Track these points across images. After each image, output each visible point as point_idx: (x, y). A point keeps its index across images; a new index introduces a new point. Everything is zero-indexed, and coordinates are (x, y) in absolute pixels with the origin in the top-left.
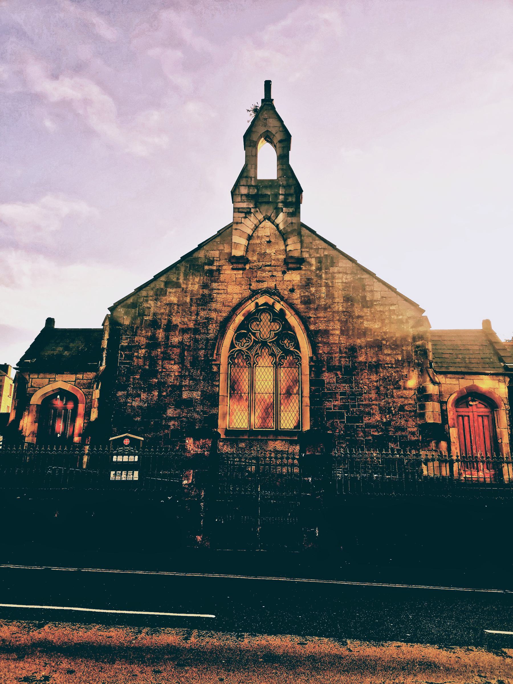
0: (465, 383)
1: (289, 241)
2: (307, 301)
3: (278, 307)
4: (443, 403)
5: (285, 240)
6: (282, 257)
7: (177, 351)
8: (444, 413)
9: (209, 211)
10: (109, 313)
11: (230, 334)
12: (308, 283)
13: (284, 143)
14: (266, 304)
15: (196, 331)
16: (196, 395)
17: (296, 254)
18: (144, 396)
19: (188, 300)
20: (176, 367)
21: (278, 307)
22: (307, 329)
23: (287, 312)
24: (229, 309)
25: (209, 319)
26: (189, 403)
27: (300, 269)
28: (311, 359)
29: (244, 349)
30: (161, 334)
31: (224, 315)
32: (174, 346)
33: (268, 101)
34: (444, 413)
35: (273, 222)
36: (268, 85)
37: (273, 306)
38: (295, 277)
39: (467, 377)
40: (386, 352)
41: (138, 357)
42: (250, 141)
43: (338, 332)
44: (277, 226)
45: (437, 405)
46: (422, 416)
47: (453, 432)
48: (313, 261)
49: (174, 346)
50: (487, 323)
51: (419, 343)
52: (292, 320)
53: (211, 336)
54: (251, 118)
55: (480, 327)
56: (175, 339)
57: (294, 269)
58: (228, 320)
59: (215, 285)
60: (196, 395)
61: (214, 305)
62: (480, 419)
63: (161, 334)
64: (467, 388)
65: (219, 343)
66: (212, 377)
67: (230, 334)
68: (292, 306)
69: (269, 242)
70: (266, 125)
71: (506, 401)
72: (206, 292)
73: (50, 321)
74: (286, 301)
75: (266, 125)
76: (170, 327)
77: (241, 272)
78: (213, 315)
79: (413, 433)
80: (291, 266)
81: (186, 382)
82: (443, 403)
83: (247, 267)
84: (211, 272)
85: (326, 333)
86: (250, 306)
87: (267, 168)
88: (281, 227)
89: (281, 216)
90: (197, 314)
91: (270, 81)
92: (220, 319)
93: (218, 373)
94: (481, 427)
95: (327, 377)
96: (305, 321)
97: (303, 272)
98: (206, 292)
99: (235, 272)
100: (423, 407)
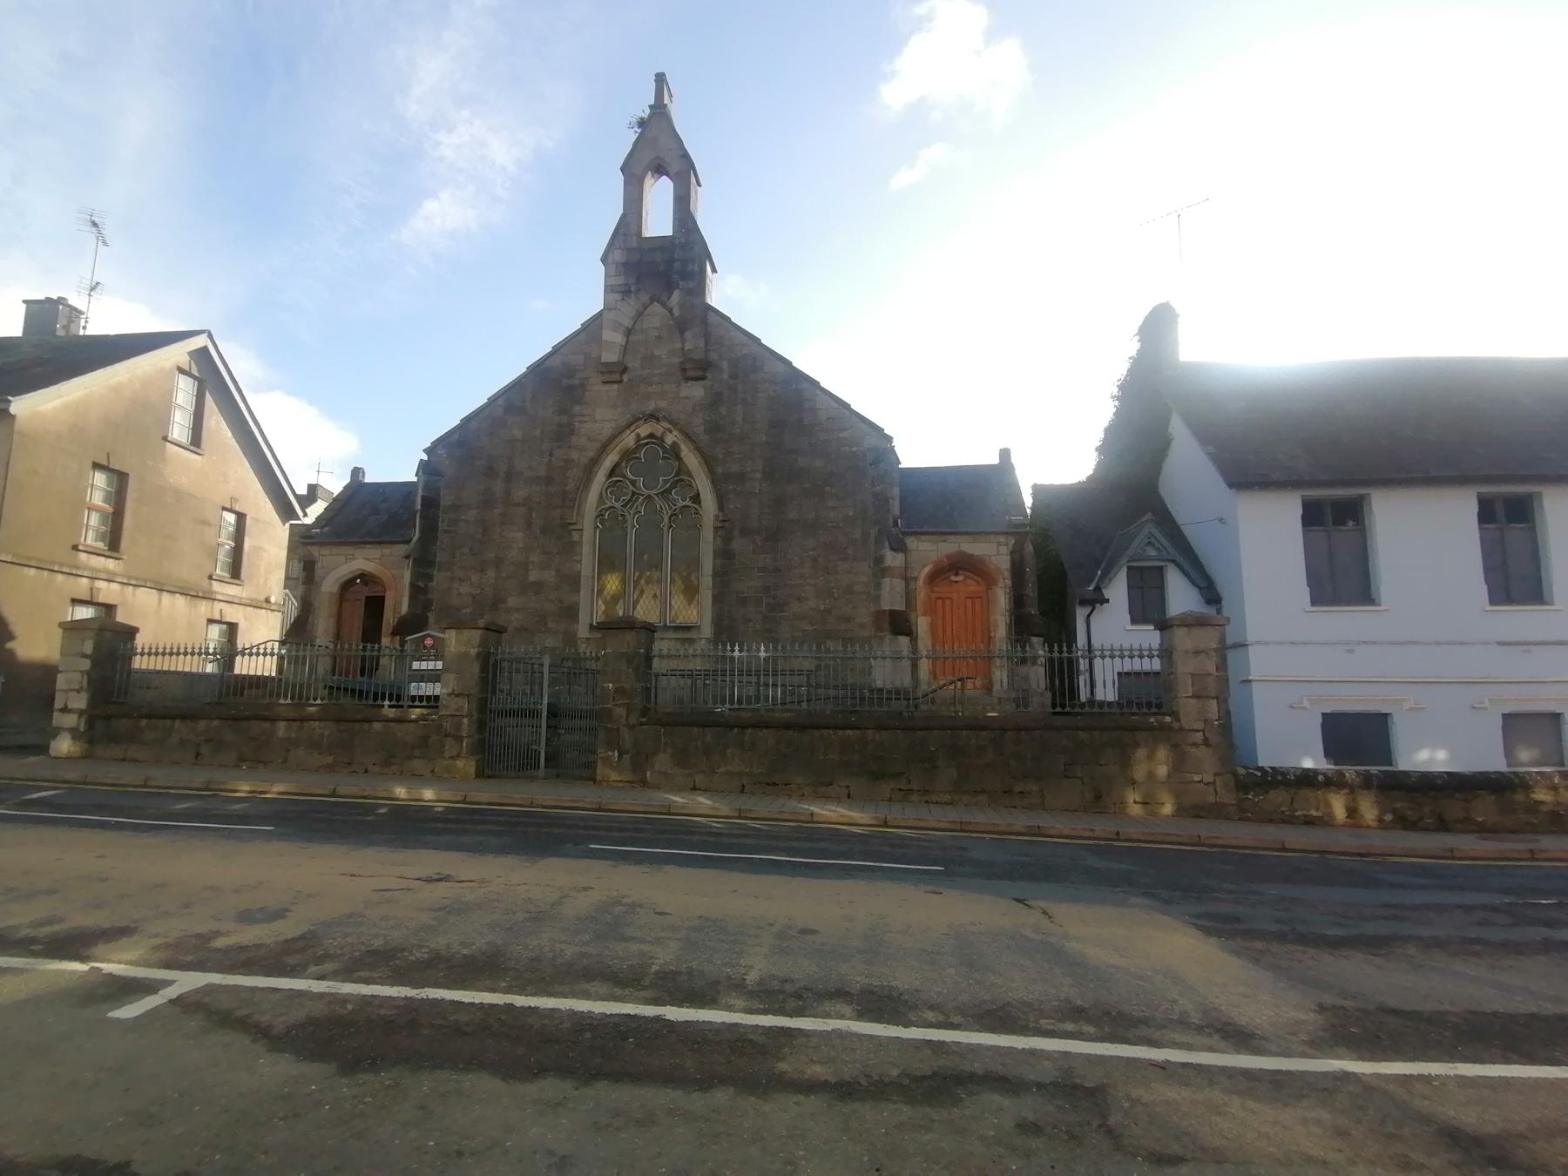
0: (949, 547)
1: (688, 335)
2: (714, 428)
3: (669, 439)
4: (908, 580)
5: (682, 333)
6: (677, 360)
7: (521, 510)
8: (909, 597)
9: (567, 297)
10: (425, 457)
11: (600, 477)
12: (715, 401)
13: (683, 172)
14: (651, 436)
15: (549, 480)
16: (549, 576)
17: (698, 355)
18: (475, 578)
19: (538, 433)
20: (520, 535)
21: (669, 439)
22: (711, 472)
23: (683, 447)
24: (598, 445)
25: (568, 462)
26: (538, 586)
27: (703, 378)
28: (716, 517)
29: (618, 505)
30: (498, 487)
31: (591, 454)
32: (518, 504)
33: (659, 110)
34: (909, 597)
35: (664, 305)
36: (660, 79)
37: (662, 439)
38: (696, 391)
39: (951, 538)
40: (830, 504)
41: (467, 522)
42: (635, 172)
43: (758, 476)
44: (670, 311)
45: (899, 584)
46: (877, 598)
47: (922, 624)
48: (725, 365)
49: (518, 504)
50: (1005, 454)
51: (878, 488)
52: (691, 459)
53: (570, 487)
54: (634, 137)
55: (995, 460)
56: (520, 493)
57: (696, 379)
58: (595, 462)
59: (577, 409)
60: (549, 576)
61: (574, 440)
62: (969, 602)
63: (498, 487)
64: (948, 557)
65: (740, 836)
66: (571, 548)
67: (600, 477)
68: (689, 437)
69: (659, 337)
70: (658, 151)
71: (1007, 574)
72: (564, 419)
73: (357, 472)
74: (681, 431)
75: (658, 151)
76: (510, 476)
77: (616, 386)
78: (574, 455)
79: (862, 626)
80: (690, 374)
81: (534, 557)
82: (908, 580)
83: (625, 378)
84: (571, 388)
85: (741, 477)
86: (629, 440)
87: (658, 222)
88: (676, 312)
89: (676, 295)
90: (551, 455)
91: (663, 74)
92: (584, 461)
93: (580, 543)
94: (969, 614)
95: (738, 544)
96: (708, 462)
97: (707, 383)
98: (564, 419)
99: (607, 387)
100: (878, 586)
